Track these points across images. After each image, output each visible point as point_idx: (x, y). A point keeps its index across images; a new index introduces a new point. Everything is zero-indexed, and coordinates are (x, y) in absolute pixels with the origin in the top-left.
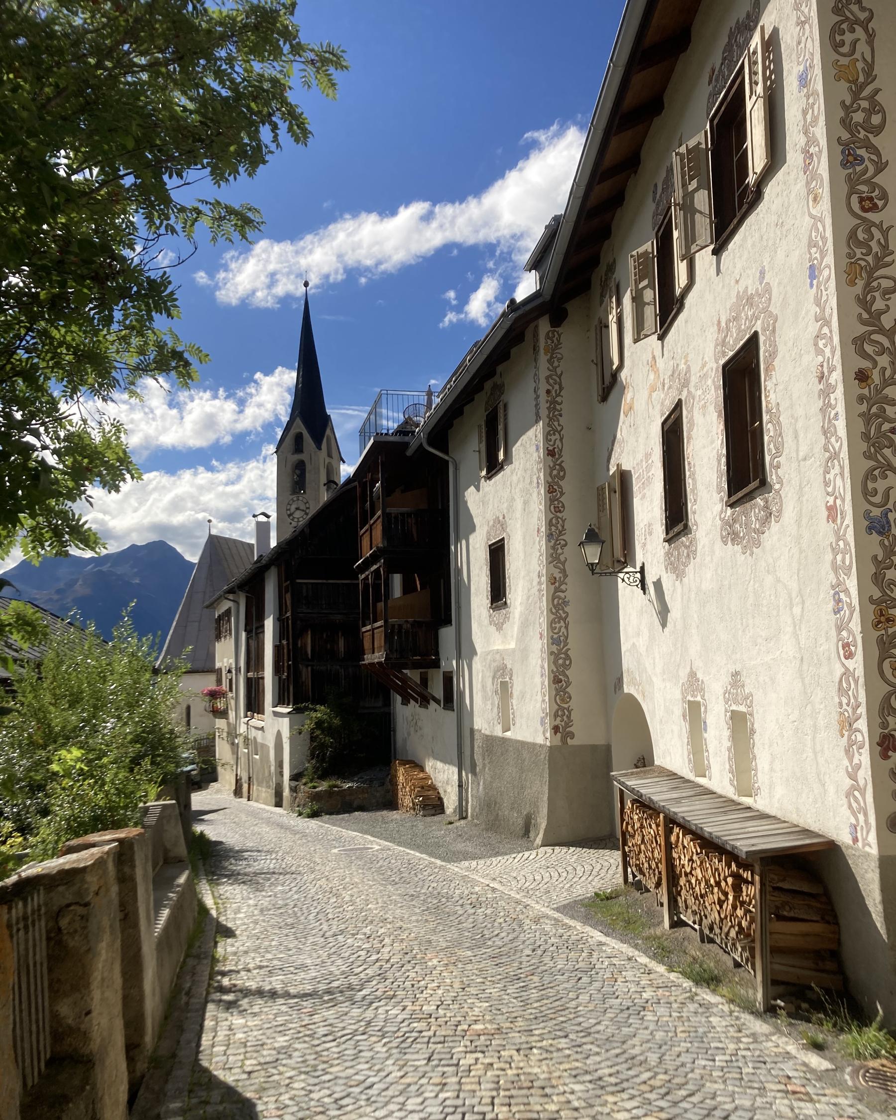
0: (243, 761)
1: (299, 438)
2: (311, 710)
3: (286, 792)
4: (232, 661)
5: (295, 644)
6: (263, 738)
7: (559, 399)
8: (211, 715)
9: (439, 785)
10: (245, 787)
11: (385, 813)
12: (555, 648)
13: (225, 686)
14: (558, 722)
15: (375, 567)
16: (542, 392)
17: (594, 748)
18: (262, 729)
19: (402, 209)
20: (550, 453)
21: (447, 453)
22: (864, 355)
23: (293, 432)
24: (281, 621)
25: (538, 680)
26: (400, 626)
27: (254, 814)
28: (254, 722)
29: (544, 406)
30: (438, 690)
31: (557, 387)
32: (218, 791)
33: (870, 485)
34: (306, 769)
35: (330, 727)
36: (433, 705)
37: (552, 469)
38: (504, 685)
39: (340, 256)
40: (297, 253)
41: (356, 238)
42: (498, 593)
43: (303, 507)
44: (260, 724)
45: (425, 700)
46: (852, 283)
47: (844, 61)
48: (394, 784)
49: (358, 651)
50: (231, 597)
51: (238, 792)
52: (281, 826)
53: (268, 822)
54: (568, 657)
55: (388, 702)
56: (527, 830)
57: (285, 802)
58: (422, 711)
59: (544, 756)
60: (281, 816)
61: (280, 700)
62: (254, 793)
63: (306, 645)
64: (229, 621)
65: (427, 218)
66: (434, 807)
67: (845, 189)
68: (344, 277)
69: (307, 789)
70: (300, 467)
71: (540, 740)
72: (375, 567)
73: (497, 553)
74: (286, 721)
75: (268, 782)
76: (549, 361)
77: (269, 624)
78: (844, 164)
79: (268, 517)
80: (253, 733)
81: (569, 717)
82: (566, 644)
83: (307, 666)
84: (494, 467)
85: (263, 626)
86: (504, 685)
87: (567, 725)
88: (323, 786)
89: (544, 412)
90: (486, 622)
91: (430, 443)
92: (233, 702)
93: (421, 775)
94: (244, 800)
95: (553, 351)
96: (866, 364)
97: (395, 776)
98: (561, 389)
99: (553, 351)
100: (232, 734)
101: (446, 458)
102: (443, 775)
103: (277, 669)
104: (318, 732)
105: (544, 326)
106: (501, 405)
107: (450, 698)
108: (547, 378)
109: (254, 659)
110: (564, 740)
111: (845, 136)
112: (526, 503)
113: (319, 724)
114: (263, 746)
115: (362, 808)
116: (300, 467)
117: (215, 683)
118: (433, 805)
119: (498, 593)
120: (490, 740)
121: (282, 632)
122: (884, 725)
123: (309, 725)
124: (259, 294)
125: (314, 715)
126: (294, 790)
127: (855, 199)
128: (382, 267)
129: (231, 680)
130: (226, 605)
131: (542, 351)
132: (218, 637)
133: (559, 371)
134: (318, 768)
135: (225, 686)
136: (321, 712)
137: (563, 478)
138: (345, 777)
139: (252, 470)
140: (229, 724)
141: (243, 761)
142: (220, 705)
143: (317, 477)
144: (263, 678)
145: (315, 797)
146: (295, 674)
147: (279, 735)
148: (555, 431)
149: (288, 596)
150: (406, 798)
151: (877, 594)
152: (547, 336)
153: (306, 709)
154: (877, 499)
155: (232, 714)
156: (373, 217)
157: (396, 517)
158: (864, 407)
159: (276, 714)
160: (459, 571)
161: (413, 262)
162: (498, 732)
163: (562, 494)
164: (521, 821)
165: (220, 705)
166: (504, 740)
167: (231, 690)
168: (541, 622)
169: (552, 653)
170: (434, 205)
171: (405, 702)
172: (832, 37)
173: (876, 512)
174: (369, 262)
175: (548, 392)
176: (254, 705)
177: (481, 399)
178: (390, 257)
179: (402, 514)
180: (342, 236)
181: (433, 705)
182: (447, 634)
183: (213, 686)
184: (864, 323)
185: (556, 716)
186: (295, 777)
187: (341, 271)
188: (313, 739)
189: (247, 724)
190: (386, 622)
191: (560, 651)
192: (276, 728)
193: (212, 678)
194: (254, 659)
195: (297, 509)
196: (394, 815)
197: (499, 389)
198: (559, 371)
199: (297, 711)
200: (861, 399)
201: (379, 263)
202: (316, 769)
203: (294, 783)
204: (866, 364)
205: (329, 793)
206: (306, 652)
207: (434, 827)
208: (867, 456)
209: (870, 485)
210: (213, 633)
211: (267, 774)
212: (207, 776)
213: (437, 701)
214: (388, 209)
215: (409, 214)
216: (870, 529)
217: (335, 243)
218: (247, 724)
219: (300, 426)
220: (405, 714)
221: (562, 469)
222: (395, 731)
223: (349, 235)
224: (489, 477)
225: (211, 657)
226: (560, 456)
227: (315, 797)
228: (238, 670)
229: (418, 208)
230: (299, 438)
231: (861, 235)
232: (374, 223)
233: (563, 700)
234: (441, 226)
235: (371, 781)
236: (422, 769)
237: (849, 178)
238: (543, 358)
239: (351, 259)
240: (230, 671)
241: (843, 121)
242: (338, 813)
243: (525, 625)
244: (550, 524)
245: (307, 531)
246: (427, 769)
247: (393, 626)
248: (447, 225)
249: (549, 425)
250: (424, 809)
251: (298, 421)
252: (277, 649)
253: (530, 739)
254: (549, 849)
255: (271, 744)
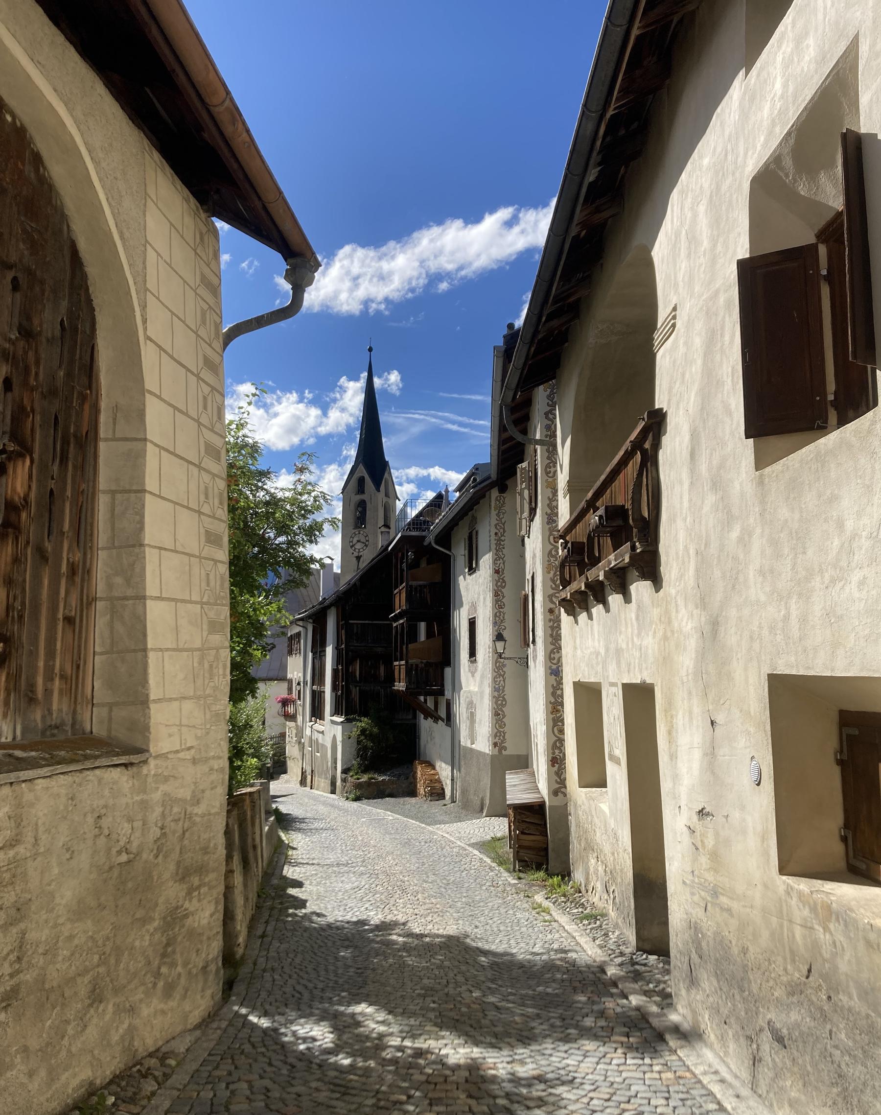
0: (308, 757)
1: (361, 481)
2: (358, 720)
3: (339, 783)
4: (301, 675)
5: (347, 670)
6: (323, 739)
7: (503, 538)
8: (283, 718)
9: (443, 779)
10: (309, 778)
11: (407, 799)
12: (496, 694)
13: (294, 695)
14: (497, 740)
15: (401, 621)
16: (493, 534)
17: (519, 756)
18: (322, 732)
19: (487, 216)
20: (497, 572)
21: (450, 550)
22: (552, 602)
23: (357, 475)
24: (337, 649)
25: (487, 713)
26: (417, 665)
27: (316, 799)
28: (317, 726)
29: (493, 542)
30: (443, 713)
31: (502, 530)
32: (287, 782)
33: (552, 656)
34: (353, 765)
35: (371, 735)
36: (440, 722)
37: (497, 582)
38: (472, 713)
39: (422, 262)
40: (380, 259)
41: (439, 244)
42: (472, 653)
43: (363, 540)
44: (321, 728)
45: (437, 719)
46: (549, 573)
47: (550, 480)
48: (415, 778)
49: (391, 679)
50: (301, 623)
51: (303, 782)
52: (332, 806)
53: (325, 804)
54: (504, 699)
55: (415, 717)
56: (482, 810)
57: (338, 790)
58: (435, 724)
59: (489, 760)
60: (334, 799)
61: (336, 711)
62: (315, 783)
63: (355, 670)
64: (299, 642)
65: (510, 224)
66: (438, 794)
67: (548, 533)
68: (426, 281)
69: (353, 780)
70: (362, 505)
71: (487, 751)
72: (401, 621)
73: (472, 624)
74: (340, 727)
75: (326, 775)
76: (498, 515)
77: (329, 651)
78: (548, 523)
79: (332, 559)
80: (316, 735)
81: (504, 737)
82: (503, 691)
83: (356, 687)
84: (472, 570)
85: (325, 651)
86: (472, 713)
87: (502, 742)
88: (364, 778)
89: (493, 547)
90: (467, 669)
91: (436, 543)
92: (301, 709)
93: (432, 772)
94: (308, 789)
95: (499, 509)
96: (552, 606)
97: (416, 772)
98: (504, 531)
99: (499, 509)
100: (300, 733)
101: (448, 552)
102: (444, 771)
103: (334, 688)
104: (362, 738)
105: (495, 493)
106: (474, 532)
107: (449, 719)
108: (496, 525)
109: (318, 676)
110: (500, 751)
111: (549, 511)
112: (484, 599)
113: (363, 731)
114: (323, 745)
115: (391, 795)
116: (362, 505)
117: (286, 691)
118: (437, 794)
119: (472, 653)
120: (465, 748)
121: (339, 658)
122: (554, 753)
123: (355, 732)
124: (343, 296)
125: (359, 724)
126: (344, 780)
127: (552, 538)
128: (463, 273)
129: (299, 691)
130: (296, 629)
131: (493, 508)
132: (290, 653)
133: (503, 521)
134: (361, 765)
135: (294, 695)
136: (364, 722)
137: (504, 587)
138: (381, 772)
139: (331, 471)
140: (297, 725)
141: (308, 757)
142: (291, 710)
143: (375, 517)
144: (324, 692)
145: (358, 786)
146: (347, 692)
147: (334, 737)
148: (500, 558)
149: (343, 632)
150: (421, 790)
151: (553, 700)
152: (496, 499)
153: (354, 720)
154: (555, 662)
155: (300, 718)
156: (459, 223)
157: (416, 588)
158: (551, 623)
159: (333, 722)
160: (455, 630)
161: (495, 267)
162: (469, 745)
163: (504, 597)
164: (479, 803)
165: (291, 710)
166: (471, 749)
167: (299, 698)
168: (489, 676)
169: (494, 697)
170: (519, 210)
171: (426, 718)
172: (546, 469)
173: (554, 667)
174: (450, 267)
175: (496, 534)
176: (317, 712)
177: (467, 519)
178: (470, 264)
179: (420, 586)
180: (425, 242)
181: (440, 722)
182: (448, 671)
183: (284, 695)
184: (553, 589)
185: (496, 736)
186: (345, 771)
187: (424, 276)
188: (359, 742)
189: (311, 727)
190: (407, 662)
191: (499, 696)
192: (331, 733)
193: (285, 685)
194: (318, 676)
195: (358, 541)
196: (413, 800)
197: (474, 520)
198: (503, 521)
199: (348, 720)
200: (550, 620)
201: (461, 268)
202: (360, 765)
203: (344, 776)
204: (552, 606)
205: (368, 784)
206: (355, 676)
207: (436, 808)
208: (552, 644)
209: (552, 656)
210: (286, 650)
211: (325, 768)
212: (278, 767)
213: (443, 720)
214: (473, 217)
215: (491, 222)
216: (551, 674)
217: (417, 250)
218: (311, 727)
219: (362, 471)
220: (425, 724)
221: (504, 581)
222: (419, 739)
223: (432, 241)
224: (470, 575)
225: (284, 667)
226: (503, 573)
227: (358, 786)
228: (305, 683)
229: (504, 213)
230: (361, 481)
231: (553, 553)
232: (459, 230)
233: (500, 727)
234: (523, 232)
235: (400, 775)
236: (434, 768)
237: (553, 719)
238: (494, 513)
239: (433, 266)
240: (299, 684)
241: (548, 505)
242: (374, 798)
243: (483, 677)
244: (495, 616)
245: (358, 584)
246: (437, 767)
247: (412, 665)
248: (530, 230)
249: (496, 554)
250: (431, 796)
251: (361, 467)
252: (335, 672)
253: (483, 750)
254: (488, 819)
255: (329, 746)
